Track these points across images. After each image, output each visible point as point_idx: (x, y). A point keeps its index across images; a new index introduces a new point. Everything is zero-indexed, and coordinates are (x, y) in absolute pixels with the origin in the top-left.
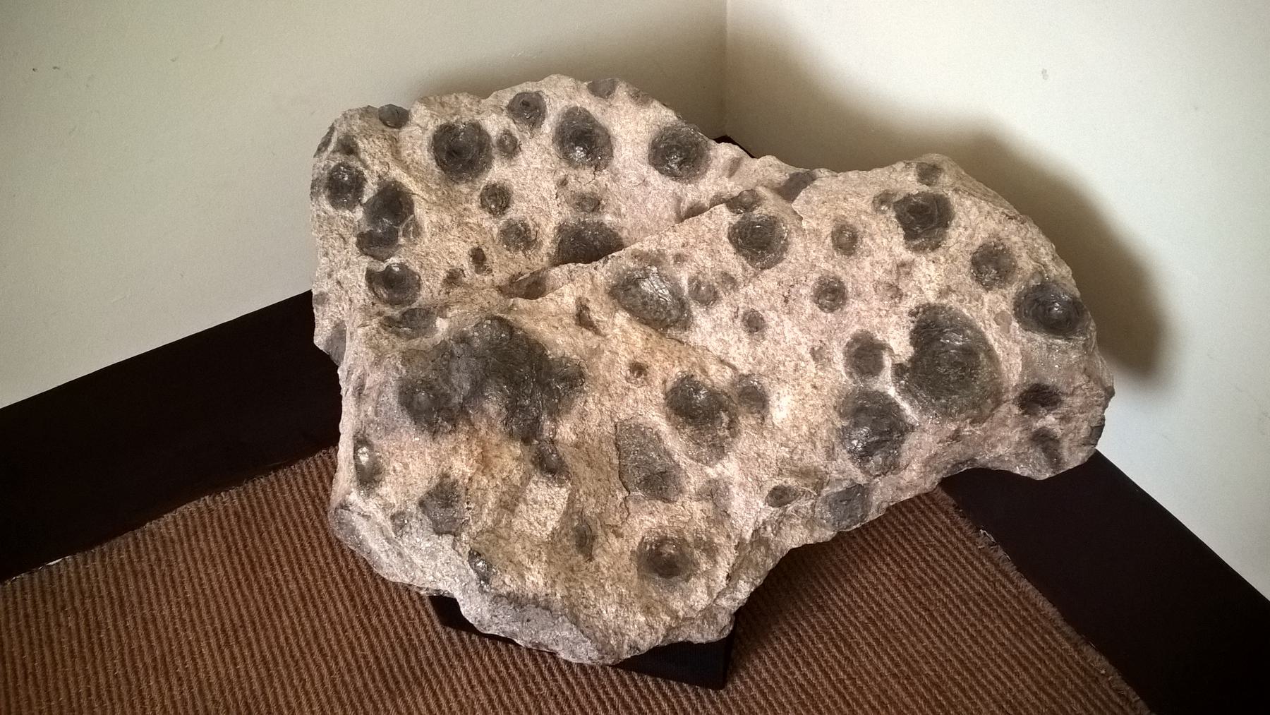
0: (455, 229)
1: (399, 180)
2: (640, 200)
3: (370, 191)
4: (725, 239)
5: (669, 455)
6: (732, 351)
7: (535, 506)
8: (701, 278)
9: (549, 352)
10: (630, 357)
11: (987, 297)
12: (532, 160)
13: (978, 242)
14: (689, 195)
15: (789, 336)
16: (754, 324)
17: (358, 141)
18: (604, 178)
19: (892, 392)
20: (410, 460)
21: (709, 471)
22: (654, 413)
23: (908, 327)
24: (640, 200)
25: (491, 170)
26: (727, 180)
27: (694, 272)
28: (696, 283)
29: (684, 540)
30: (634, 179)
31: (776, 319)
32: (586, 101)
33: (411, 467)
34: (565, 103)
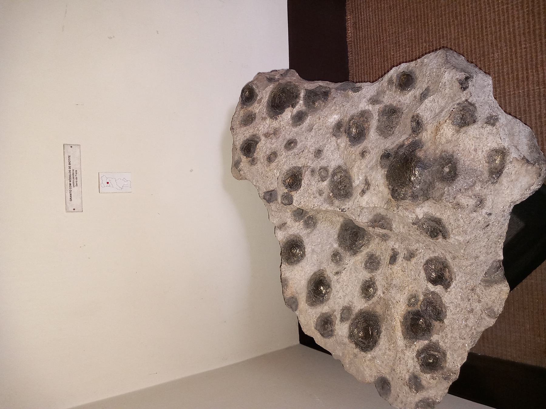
0: (393, 284)
1: (402, 338)
2: (320, 246)
3: (421, 344)
4: (302, 188)
5: (379, 120)
6: (332, 149)
7: (432, 109)
8: (320, 179)
9: (386, 172)
10: (362, 161)
11: (257, 111)
12: (342, 297)
13: (245, 128)
14: (304, 233)
15: (313, 141)
16: (318, 153)
17: (407, 380)
18: (323, 266)
19: (301, 102)
20: (471, 151)
21: (370, 109)
22: (372, 137)
23: (281, 116)
24: (320, 246)
25: (362, 308)
26: (288, 223)
27: (321, 182)
28: (323, 179)
29: (396, 87)
30: (315, 256)
31: (311, 148)
32: (303, 304)
33: (473, 148)
34: (310, 310)
